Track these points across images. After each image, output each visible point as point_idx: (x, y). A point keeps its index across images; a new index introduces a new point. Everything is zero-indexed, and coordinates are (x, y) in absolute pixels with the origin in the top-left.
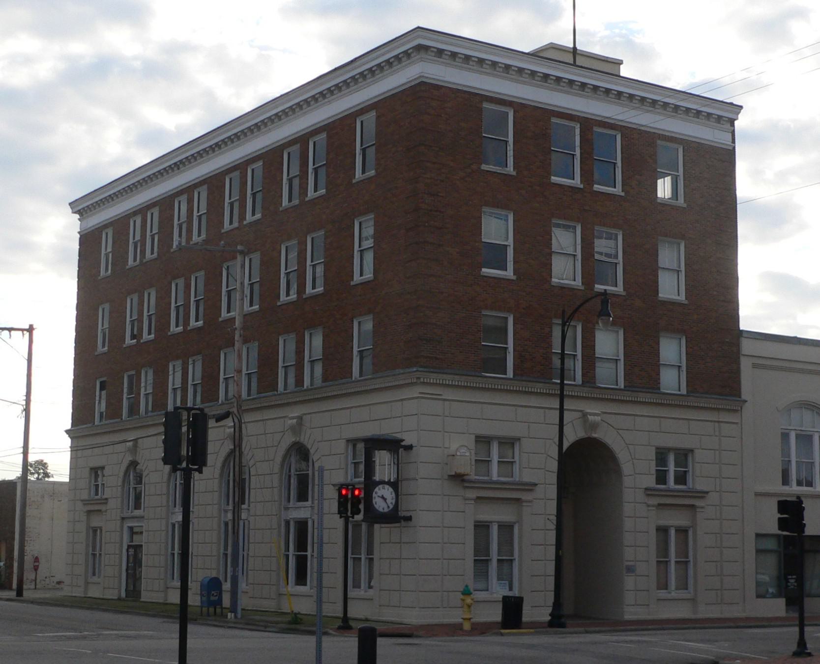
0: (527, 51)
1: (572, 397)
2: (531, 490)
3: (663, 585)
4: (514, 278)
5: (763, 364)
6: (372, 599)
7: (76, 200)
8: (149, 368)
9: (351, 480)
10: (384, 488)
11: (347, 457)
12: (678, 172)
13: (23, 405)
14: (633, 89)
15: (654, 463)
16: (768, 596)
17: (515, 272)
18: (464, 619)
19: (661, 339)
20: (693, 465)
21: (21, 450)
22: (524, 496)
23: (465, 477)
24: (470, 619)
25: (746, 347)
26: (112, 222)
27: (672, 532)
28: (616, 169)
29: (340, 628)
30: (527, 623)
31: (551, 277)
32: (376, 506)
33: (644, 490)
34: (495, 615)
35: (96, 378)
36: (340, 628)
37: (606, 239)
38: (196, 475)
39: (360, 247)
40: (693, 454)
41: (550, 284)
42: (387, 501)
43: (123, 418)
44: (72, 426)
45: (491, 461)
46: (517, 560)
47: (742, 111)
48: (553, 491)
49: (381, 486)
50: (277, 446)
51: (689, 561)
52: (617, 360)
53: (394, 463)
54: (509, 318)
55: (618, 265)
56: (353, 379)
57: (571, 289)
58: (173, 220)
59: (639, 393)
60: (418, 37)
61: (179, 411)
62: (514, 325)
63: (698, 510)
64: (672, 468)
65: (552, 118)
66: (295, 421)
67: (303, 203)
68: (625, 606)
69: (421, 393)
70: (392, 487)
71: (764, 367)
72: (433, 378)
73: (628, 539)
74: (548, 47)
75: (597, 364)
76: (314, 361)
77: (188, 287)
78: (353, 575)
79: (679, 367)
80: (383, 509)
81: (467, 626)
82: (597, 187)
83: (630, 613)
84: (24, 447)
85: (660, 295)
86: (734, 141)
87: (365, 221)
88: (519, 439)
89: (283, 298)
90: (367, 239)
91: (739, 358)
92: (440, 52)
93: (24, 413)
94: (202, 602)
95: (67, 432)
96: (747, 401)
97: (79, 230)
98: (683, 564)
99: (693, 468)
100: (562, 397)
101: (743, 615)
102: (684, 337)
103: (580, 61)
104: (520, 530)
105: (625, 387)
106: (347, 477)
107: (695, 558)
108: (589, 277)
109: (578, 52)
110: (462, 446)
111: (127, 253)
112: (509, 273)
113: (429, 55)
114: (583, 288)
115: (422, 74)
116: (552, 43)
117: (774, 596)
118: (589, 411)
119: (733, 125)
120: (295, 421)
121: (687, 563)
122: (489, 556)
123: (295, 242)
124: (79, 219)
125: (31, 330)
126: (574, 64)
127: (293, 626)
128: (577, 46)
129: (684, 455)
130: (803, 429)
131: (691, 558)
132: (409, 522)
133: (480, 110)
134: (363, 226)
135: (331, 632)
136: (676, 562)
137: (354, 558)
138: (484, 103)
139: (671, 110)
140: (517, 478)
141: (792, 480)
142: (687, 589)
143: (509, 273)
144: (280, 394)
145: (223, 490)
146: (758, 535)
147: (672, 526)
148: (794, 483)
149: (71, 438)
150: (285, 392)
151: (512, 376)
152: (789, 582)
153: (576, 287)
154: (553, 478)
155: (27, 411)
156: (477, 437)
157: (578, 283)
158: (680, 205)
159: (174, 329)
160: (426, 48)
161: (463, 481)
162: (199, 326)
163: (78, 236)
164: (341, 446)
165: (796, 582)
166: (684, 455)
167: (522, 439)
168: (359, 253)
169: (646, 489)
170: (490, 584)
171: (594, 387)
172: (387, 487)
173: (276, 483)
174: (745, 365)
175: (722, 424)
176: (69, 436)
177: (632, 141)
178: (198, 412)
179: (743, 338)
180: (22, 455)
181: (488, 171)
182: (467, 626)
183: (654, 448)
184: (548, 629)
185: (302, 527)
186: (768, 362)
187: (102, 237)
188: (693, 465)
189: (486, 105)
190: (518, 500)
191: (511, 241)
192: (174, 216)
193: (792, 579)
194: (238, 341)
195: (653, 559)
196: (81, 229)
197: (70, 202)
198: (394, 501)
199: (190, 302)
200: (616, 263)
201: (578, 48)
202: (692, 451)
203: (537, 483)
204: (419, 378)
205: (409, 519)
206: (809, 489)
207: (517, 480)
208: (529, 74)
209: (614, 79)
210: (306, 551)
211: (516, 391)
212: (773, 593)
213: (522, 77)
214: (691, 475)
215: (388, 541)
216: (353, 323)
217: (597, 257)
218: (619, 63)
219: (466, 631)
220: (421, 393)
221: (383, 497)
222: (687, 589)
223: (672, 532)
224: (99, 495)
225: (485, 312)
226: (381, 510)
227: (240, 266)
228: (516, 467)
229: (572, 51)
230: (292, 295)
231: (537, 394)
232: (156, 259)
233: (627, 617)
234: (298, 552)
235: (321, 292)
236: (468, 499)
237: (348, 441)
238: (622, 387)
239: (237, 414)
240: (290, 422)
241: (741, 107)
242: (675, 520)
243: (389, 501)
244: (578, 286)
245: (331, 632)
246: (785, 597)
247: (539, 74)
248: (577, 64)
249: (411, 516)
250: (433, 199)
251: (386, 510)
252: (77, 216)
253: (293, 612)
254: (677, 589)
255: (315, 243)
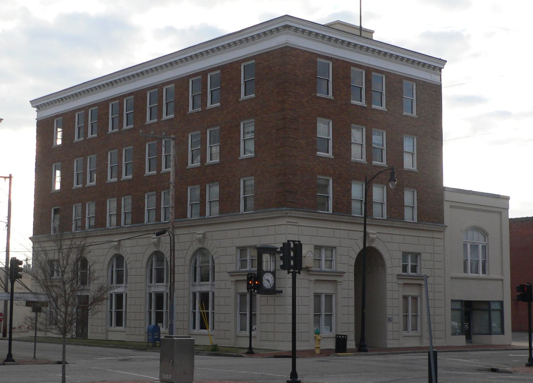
0: (323, 24)
1: (369, 224)
2: (342, 276)
3: (406, 329)
4: (333, 157)
5: (456, 206)
6: (256, 337)
7: (36, 100)
8: (91, 202)
9: (239, 269)
10: (268, 275)
11: (236, 257)
12: (413, 98)
13: (6, 223)
14: (392, 51)
15: (401, 260)
16: (456, 334)
17: (334, 154)
18: (316, 347)
19: (405, 192)
20: (420, 262)
21: (5, 249)
22: (338, 279)
23: (310, 269)
24: (319, 348)
25: (447, 196)
26: (62, 114)
27: (410, 298)
28: (329, 83)
29: (247, 353)
30: (349, 349)
31: (351, 157)
32: (265, 285)
33: (396, 276)
34: (331, 345)
35: (52, 207)
36: (247, 353)
37: (377, 135)
38: (297, 274)
39: (244, 138)
40: (336, 249)
41: (351, 160)
42: (270, 282)
43: (73, 231)
44: (33, 235)
45: (321, 259)
46: (334, 315)
47: (446, 63)
48: (352, 277)
49: (266, 274)
50: (188, 250)
51: (333, 314)
52: (382, 203)
53: (273, 261)
54: (330, 180)
55: (383, 150)
56: (240, 213)
57: (361, 164)
58: (108, 115)
59: (395, 222)
60: (286, 20)
61: (290, 242)
62: (333, 184)
63: (338, 284)
64: (410, 264)
65: (372, 72)
66: (201, 236)
67: (204, 111)
68: (387, 340)
69: (287, 222)
70: (272, 274)
71: (456, 207)
72: (294, 213)
73: (389, 303)
74: (336, 22)
75: (374, 206)
76: (211, 201)
77: (120, 155)
78: (241, 322)
79: (413, 207)
80: (268, 286)
81: (318, 351)
82: (373, 106)
83: (391, 344)
84: (7, 248)
85: (405, 167)
86: (441, 81)
87: (247, 123)
88: (336, 248)
89: (190, 165)
90: (248, 133)
91: (443, 202)
92: (297, 29)
93: (7, 227)
94: (148, 339)
95: (30, 238)
96: (447, 226)
97: (36, 118)
98: (329, 316)
99: (420, 264)
100: (365, 225)
101: (445, 345)
102: (416, 191)
103: (363, 34)
104: (336, 299)
105: (387, 218)
106: (237, 268)
107: (336, 314)
108: (370, 158)
109: (362, 29)
110: (309, 251)
111: (74, 133)
112: (330, 155)
113: (291, 31)
114: (366, 163)
115: (287, 42)
116: (338, 21)
117: (459, 334)
118: (370, 232)
119: (440, 71)
120: (201, 236)
121: (416, 316)
122: (320, 313)
123: (199, 132)
124: (36, 111)
125: (10, 177)
126: (361, 36)
127: (214, 352)
128: (362, 25)
129: (416, 256)
130: (474, 241)
131: (419, 314)
132: (281, 293)
133: (316, 63)
134: (246, 126)
135: (244, 355)
136: (412, 315)
137: (241, 314)
138: (318, 58)
139: (421, 65)
140: (334, 269)
141: (468, 270)
142: (417, 330)
143: (330, 155)
144: (188, 220)
145: (148, 274)
146: (452, 301)
147: (410, 296)
148: (469, 272)
149: (33, 242)
150: (191, 219)
151: (331, 212)
152: (465, 326)
153: (362, 163)
154: (352, 269)
155: (8, 225)
156: (315, 246)
157: (364, 160)
158: (415, 117)
159: (111, 180)
160: (289, 27)
161: (308, 271)
162: (129, 178)
163: (36, 121)
164: (233, 250)
165: (468, 326)
166: (416, 256)
167: (338, 248)
168: (243, 141)
169: (398, 275)
170: (321, 328)
171: (372, 219)
172: (269, 274)
173: (187, 271)
174: (446, 206)
175: (435, 239)
176: (32, 241)
177: (391, 80)
178: (298, 243)
179: (445, 191)
180: (6, 252)
181: (320, 97)
182: (318, 351)
183: (401, 252)
184: (358, 353)
185: (205, 297)
186: (466, 206)
187: (54, 123)
188: (420, 262)
189: (319, 60)
190: (335, 281)
191: (331, 137)
192: (109, 113)
193: (466, 324)
194: (172, 190)
195: (401, 314)
196: (37, 117)
197: (31, 100)
198: (273, 282)
199: (122, 164)
200: (328, 139)
201: (363, 27)
202: (420, 254)
203: (345, 271)
204: (286, 214)
205: (281, 292)
206: (477, 275)
207: (334, 270)
208: (353, 46)
209: (368, 41)
210: (162, 309)
211: (360, 223)
212: (459, 332)
213: (337, 44)
214: (419, 267)
215: (266, 304)
216: (240, 181)
217: (373, 145)
218: (372, 32)
219: (317, 354)
220: (287, 222)
221: (268, 280)
222: (417, 330)
223: (410, 298)
224: (55, 276)
225: (319, 177)
226: (267, 287)
227: (173, 147)
228: (334, 263)
229: (359, 28)
230: (196, 163)
231: (344, 222)
232: (96, 138)
233: (389, 346)
234: (117, 309)
235: (218, 163)
236: (311, 281)
237: (237, 248)
238: (386, 218)
239: (172, 232)
240: (198, 236)
241: (446, 61)
242: (412, 292)
243: (271, 282)
244: (364, 162)
245: (244, 355)
246: (465, 335)
247: (352, 44)
248: (362, 36)
249: (282, 291)
250: (292, 112)
251: (269, 287)
252: (36, 109)
253: (213, 344)
254: (412, 330)
255: (92, 112)
